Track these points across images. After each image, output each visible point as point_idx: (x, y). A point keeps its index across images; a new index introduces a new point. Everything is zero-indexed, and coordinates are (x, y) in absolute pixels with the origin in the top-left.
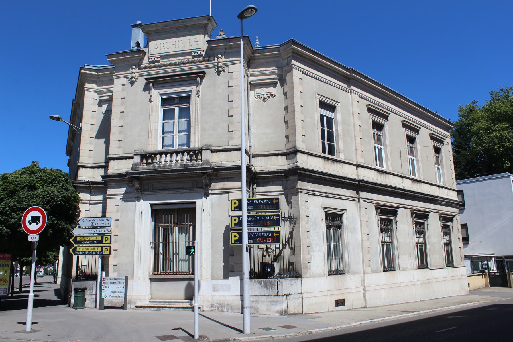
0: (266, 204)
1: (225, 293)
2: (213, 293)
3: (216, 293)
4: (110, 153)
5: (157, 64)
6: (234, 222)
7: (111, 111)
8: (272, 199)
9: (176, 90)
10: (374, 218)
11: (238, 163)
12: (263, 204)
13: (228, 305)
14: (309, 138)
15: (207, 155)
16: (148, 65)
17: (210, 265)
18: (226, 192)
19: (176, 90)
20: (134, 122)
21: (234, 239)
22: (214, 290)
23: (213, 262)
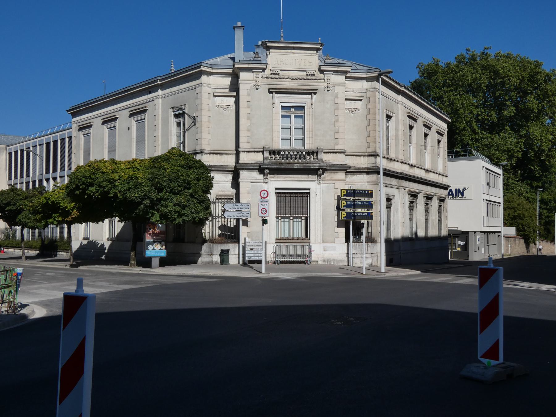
0: (364, 193)
1: (332, 252)
2: (324, 252)
3: (326, 252)
4: (240, 146)
5: (277, 76)
6: (343, 194)
7: (387, 207)
8: (368, 191)
9: (293, 96)
10: (407, 198)
11: (361, 265)
12: (362, 193)
13: (334, 260)
14: (249, 244)
15: (322, 156)
16: (270, 76)
17: (321, 233)
18: (334, 181)
19: (293, 96)
20: (268, 128)
21: (343, 205)
22: (325, 251)
23: (323, 231)
